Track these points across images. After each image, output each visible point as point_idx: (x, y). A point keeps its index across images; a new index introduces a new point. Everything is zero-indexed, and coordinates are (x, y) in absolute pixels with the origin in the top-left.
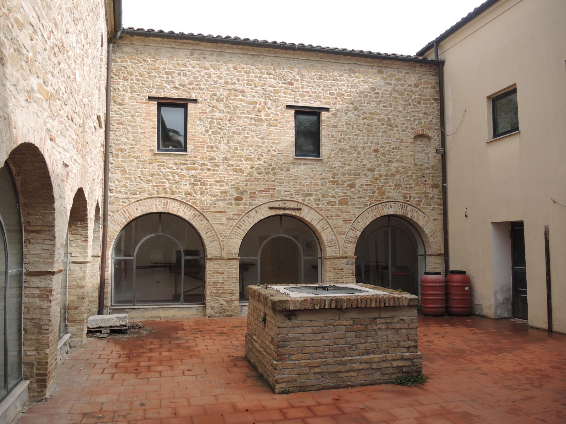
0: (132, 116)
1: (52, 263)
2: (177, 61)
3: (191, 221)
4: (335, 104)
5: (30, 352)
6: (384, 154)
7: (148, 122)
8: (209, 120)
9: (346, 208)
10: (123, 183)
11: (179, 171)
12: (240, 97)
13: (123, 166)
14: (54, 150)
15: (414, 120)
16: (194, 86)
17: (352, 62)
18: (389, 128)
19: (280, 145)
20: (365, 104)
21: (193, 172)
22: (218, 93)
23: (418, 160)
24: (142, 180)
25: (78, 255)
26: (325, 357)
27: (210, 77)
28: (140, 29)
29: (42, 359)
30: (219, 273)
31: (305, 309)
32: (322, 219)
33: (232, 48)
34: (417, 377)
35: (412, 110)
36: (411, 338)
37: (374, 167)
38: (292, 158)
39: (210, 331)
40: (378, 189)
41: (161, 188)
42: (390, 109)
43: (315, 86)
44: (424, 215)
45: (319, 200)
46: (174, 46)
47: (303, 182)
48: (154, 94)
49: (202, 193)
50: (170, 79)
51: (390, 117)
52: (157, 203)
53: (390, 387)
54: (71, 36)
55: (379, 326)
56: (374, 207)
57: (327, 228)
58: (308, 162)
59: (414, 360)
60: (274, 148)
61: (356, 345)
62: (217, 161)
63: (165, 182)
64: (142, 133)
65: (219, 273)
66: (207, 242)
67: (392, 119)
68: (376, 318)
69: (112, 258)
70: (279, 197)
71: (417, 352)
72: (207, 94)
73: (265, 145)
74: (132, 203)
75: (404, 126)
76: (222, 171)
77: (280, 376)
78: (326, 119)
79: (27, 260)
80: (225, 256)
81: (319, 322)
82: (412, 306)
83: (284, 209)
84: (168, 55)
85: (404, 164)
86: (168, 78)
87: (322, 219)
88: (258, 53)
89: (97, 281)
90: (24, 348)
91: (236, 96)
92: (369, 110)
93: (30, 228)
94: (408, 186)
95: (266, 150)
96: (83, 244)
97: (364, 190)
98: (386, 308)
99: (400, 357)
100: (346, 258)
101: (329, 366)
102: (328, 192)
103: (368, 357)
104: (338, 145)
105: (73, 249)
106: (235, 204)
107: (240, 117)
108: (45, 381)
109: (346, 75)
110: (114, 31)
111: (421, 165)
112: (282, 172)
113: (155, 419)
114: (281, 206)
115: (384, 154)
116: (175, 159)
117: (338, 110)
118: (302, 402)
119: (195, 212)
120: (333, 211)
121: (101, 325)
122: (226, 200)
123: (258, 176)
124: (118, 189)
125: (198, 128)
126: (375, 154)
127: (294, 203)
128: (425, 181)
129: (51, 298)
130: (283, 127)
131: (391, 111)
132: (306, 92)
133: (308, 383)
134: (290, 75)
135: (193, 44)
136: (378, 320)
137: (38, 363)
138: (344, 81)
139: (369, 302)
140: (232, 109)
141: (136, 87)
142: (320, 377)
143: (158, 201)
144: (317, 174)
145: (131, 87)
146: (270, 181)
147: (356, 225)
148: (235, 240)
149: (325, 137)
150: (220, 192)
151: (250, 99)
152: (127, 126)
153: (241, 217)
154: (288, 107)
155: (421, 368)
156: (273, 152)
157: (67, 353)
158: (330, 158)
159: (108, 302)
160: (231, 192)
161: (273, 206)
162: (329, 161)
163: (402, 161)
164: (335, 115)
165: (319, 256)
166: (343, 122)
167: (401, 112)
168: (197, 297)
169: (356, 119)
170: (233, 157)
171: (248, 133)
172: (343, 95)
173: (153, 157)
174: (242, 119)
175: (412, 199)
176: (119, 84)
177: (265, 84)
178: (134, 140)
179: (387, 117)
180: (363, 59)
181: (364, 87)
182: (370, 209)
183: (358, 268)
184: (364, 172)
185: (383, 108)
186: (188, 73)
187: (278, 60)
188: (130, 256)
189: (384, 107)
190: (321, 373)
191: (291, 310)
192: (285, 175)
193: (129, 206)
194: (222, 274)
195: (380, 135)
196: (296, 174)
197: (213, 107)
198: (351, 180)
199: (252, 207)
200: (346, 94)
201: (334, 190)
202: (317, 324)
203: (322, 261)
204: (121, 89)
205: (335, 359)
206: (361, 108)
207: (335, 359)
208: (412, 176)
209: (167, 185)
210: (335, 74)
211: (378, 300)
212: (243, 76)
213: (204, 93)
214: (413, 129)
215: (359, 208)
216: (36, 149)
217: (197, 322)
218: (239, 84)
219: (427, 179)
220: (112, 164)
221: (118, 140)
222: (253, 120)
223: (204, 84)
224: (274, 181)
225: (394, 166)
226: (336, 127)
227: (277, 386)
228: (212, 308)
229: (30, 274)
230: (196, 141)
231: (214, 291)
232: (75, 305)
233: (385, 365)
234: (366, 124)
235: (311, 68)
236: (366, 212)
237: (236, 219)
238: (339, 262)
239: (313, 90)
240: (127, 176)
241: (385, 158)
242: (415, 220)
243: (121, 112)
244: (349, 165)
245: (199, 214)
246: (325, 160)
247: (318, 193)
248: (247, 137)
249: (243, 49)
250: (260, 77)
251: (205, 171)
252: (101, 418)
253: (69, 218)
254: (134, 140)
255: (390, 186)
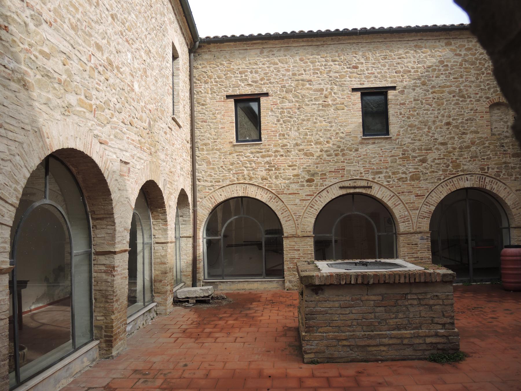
0: (213, 114)
1: (114, 244)
2: (249, 60)
3: (267, 203)
4: (402, 81)
5: (99, 317)
6: (457, 127)
7: (227, 118)
8: (280, 110)
9: (418, 183)
10: (209, 173)
11: (256, 158)
12: (308, 86)
13: (207, 158)
14: (107, 152)
15: (489, 89)
16: (265, 81)
17: (417, 39)
18: (461, 99)
19: (348, 127)
20: (434, 78)
21: (268, 159)
22: (287, 85)
23: (495, 130)
24: (224, 169)
25: (161, 236)
26: (354, 331)
27: (279, 71)
28: (260, 35)
29: (108, 323)
30: (295, 250)
31: (331, 285)
32: (394, 196)
33: (298, 42)
34: (453, 354)
35: (486, 78)
36: (446, 315)
37: (447, 140)
38: (360, 139)
39: (281, 303)
40: (452, 162)
41: (241, 175)
42: (461, 80)
43: (380, 67)
44: (505, 187)
45: (390, 177)
46: (246, 48)
47: (372, 160)
48: (230, 93)
49: (276, 178)
50: (244, 77)
51: (462, 88)
52: (238, 188)
53: (421, 363)
54: (124, 54)
55: (410, 302)
56: (449, 181)
57: (399, 204)
58: (376, 141)
59: (450, 338)
60: (342, 131)
61: (385, 320)
62: (288, 147)
63: (243, 170)
64: (222, 128)
65: (295, 250)
66: (283, 222)
67: (464, 91)
68: (407, 294)
69: (203, 238)
70: (348, 177)
71: (454, 329)
72: (277, 87)
73: (334, 128)
74: (217, 190)
75: (478, 96)
76: (294, 156)
77: (308, 347)
78: (393, 97)
79: (95, 242)
80: (300, 234)
81: (346, 297)
82: (446, 282)
83: (355, 187)
84: (241, 56)
85: (479, 135)
86: (242, 77)
87: (394, 196)
88: (322, 43)
89: (191, 258)
90: (95, 314)
91: (303, 85)
92: (438, 84)
93: (95, 216)
94: (486, 157)
95: (334, 133)
96: (164, 227)
97: (437, 164)
98: (417, 284)
99: (434, 333)
100: (420, 233)
101: (357, 340)
102: (399, 169)
103: (399, 332)
104: (407, 121)
105: (156, 231)
106: (307, 185)
107: (309, 105)
108: (111, 341)
109: (412, 52)
110: (193, 42)
111: (499, 134)
112: (351, 153)
113: (188, 378)
114: (351, 185)
115: (457, 127)
116: (251, 149)
117: (405, 87)
118: (325, 373)
119: (271, 195)
120: (404, 187)
121: (188, 296)
122: (298, 182)
123: (328, 158)
124: (205, 178)
125: (270, 119)
126: (447, 127)
127: (364, 181)
128: (505, 151)
129: (115, 273)
130: (350, 110)
131: (463, 82)
132: (371, 73)
133: (336, 355)
134: (355, 59)
135: (262, 44)
136: (409, 295)
137: (106, 326)
138: (410, 58)
139: (397, 277)
140: (301, 98)
141: (215, 88)
142: (349, 350)
143: (239, 187)
144: (385, 152)
145: (211, 89)
146: (339, 162)
147: (430, 200)
148: (309, 219)
149: (393, 115)
150: (293, 176)
151: (317, 87)
152: (210, 124)
153: (313, 197)
154: (354, 90)
155: (458, 345)
156: (341, 135)
157: (152, 319)
158: (399, 135)
159: (201, 276)
160: (303, 174)
161: (344, 185)
162: (398, 139)
163: (477, 132)
164: (402, 92)
165: (394, 232)
166: (411, 98)
167: (473, 82)
168: (276, 271)
169: (425, 94)
170: (304, 142)
171: (316, 119)
172: (410, 71)
173: (233, 148)
174: (310, 106)
175: (490, 170)
176: (201, 88)
177: (330, 71)
178: (215, 135)
179: (458, 89)
180: (428, 33)
181: (431, 61)
182: (444, 183)
183: (434, 243)
184: (435, 147)
185: (453, 80)
186: (259, 70)
187: (342, 46)
188: (217, 235)
189: (454, 78)
190: (349, 346)
191: (317, 285)
192: (354, 155)
193: (214, 193)
194: (298, 251)
195: (452, 108)
196: (365, 153)
197: (283, 98)
198: (424, 155)
199: (323, 188)
200: (412, 71)
201: (404, 166)
202: (344, 298)
203: (396, 236)
204: (203, 91)
205: (363, 333)
206: (430, 82)
207: (363, 333)
208: (489, 147)
209: (246, 172)
210: (401, 52)
211: (407, 276)
212: (309, 66)
213: (274, 87)
214: (488, 98)
215: (432, 183)
216: (81, 153)
217: (274, 295)
218: (306, 74)
219: (506, 148)
220: (199, 157)
221: (202, 136)
222: (321, 106)
223: (274, 78)
224: (344, 162)
225: (468, 137)
226: (404, 104)
227: (306, 356)
228: (290, 282)
229: (98, 254)
230: (269, 131)
231: (292, 267)
232: (160, 278)
233: (417, 341)
234: (436, 98)
235: (375, 49)
236: (440, 186)
237: (309, 200)
238: (413, 237)
239: (378, 71)
240: (211, 166)
241: (458, 130)
242: (495, 191)
243: (204, 111)
244: (420, 140)
245: (274, 196)
246: (394, 138)
247: (388, 170)
248: (315, 123)
249: (308, 41)
250: (325, 65)
251: (279, 157)
252: (147, 374)
253: (134, 207)
254: (215, 135)
255: (465, 158)
